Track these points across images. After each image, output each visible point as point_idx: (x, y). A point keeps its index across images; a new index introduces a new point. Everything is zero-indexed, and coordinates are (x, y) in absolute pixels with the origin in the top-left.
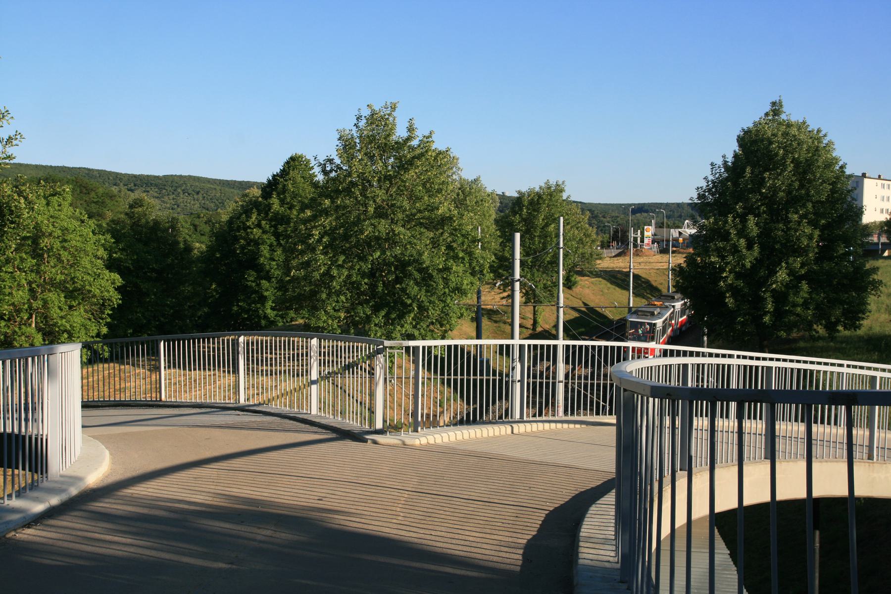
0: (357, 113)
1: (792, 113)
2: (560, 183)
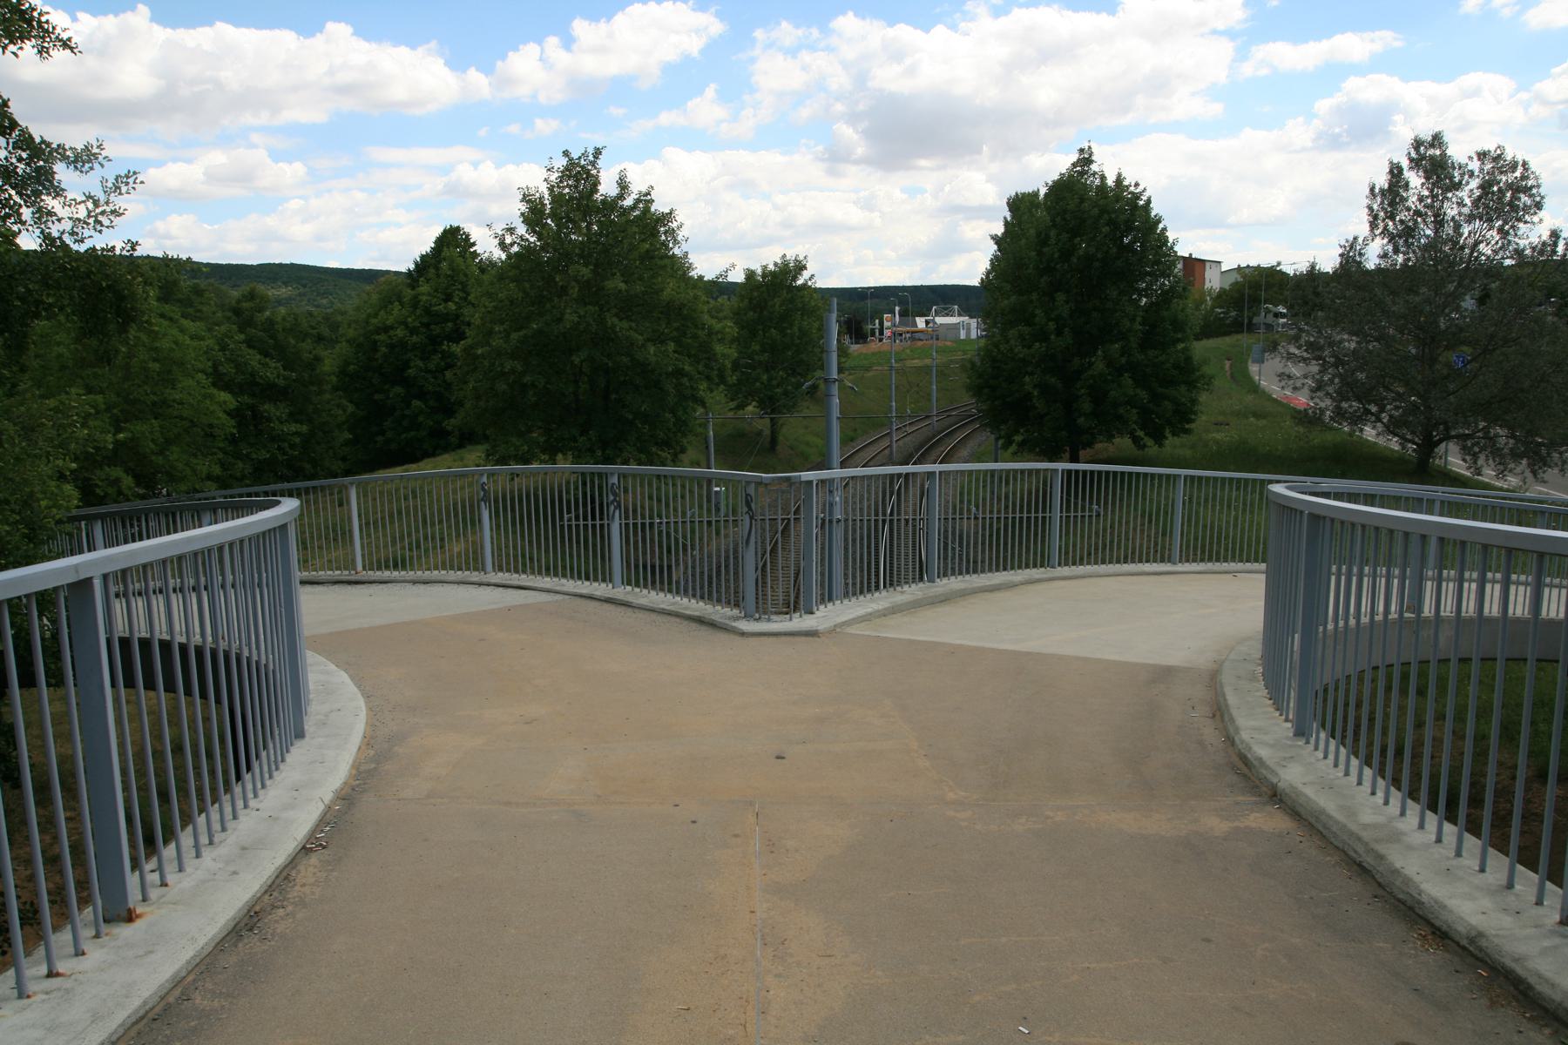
0: (547, 163)
1: (1109, 165)
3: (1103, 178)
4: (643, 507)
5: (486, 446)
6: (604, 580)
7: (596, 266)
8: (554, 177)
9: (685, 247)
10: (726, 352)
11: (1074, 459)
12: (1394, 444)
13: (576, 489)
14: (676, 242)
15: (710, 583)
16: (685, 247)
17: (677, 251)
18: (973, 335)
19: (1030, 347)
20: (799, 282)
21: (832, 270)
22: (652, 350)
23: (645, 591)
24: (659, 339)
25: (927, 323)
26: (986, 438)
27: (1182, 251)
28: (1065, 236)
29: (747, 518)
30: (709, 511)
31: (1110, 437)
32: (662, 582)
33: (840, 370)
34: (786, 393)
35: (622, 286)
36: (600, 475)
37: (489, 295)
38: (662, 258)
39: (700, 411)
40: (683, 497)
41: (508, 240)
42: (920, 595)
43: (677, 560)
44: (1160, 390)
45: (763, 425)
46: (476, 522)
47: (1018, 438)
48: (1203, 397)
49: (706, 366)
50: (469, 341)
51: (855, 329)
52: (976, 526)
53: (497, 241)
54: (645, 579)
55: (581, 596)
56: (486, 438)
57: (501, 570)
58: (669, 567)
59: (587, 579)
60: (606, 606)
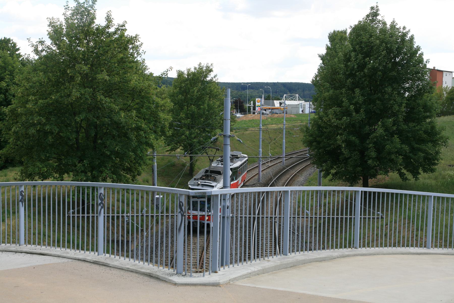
1: (387, 16)
2: (209, 65)
3: (385, 24)
4: (113, 206)
5: (21, 168)
6: (93, 250)
7: (92, 65)
8: (69, 13)
9: (143, 56)
10: (166, 117)
11: (365, 185)
12: (22, 210)
13: (74, 195)
14: (138, 54)
15: (152, 252)
16: (143, 56)
17: (139, 58)
18: (307, 111)
19: (340, 119)
20: (208, 79)
21: (227, 72)
22: (123, 114)
23: (117, 257)
24: (127, 109)
25: (281, 104)
26: (314, 171)
27: (430, 66)
28: (360, 56)
29: (180, 216)
30: (152, 209)
31: (386, 172)
32: (122, 250)
33: (231, 130)
34: (199, 142)
35: (107, 78)
36: (93, 188)
37: (28, 80)
38: (130, 62)
39: (150, 150)
40: (137, 201)
41: (40, 48)
42: (278, 263)
43: (133, 238)
44: (416, 146)
45: (186, 160)
46: (15, 212)
47: (333, 171)
48: (443, 150)
49: (154, 125)
50: (14, 106)
51: (239, 106)
52: (307, 221)
53: (33, 49)
54: (113, 248)
55: (79, 260)
56: (21, 163)
57: (29, 243)
58: (128, 242)
59: (83, 249)
60: (94, 266)
